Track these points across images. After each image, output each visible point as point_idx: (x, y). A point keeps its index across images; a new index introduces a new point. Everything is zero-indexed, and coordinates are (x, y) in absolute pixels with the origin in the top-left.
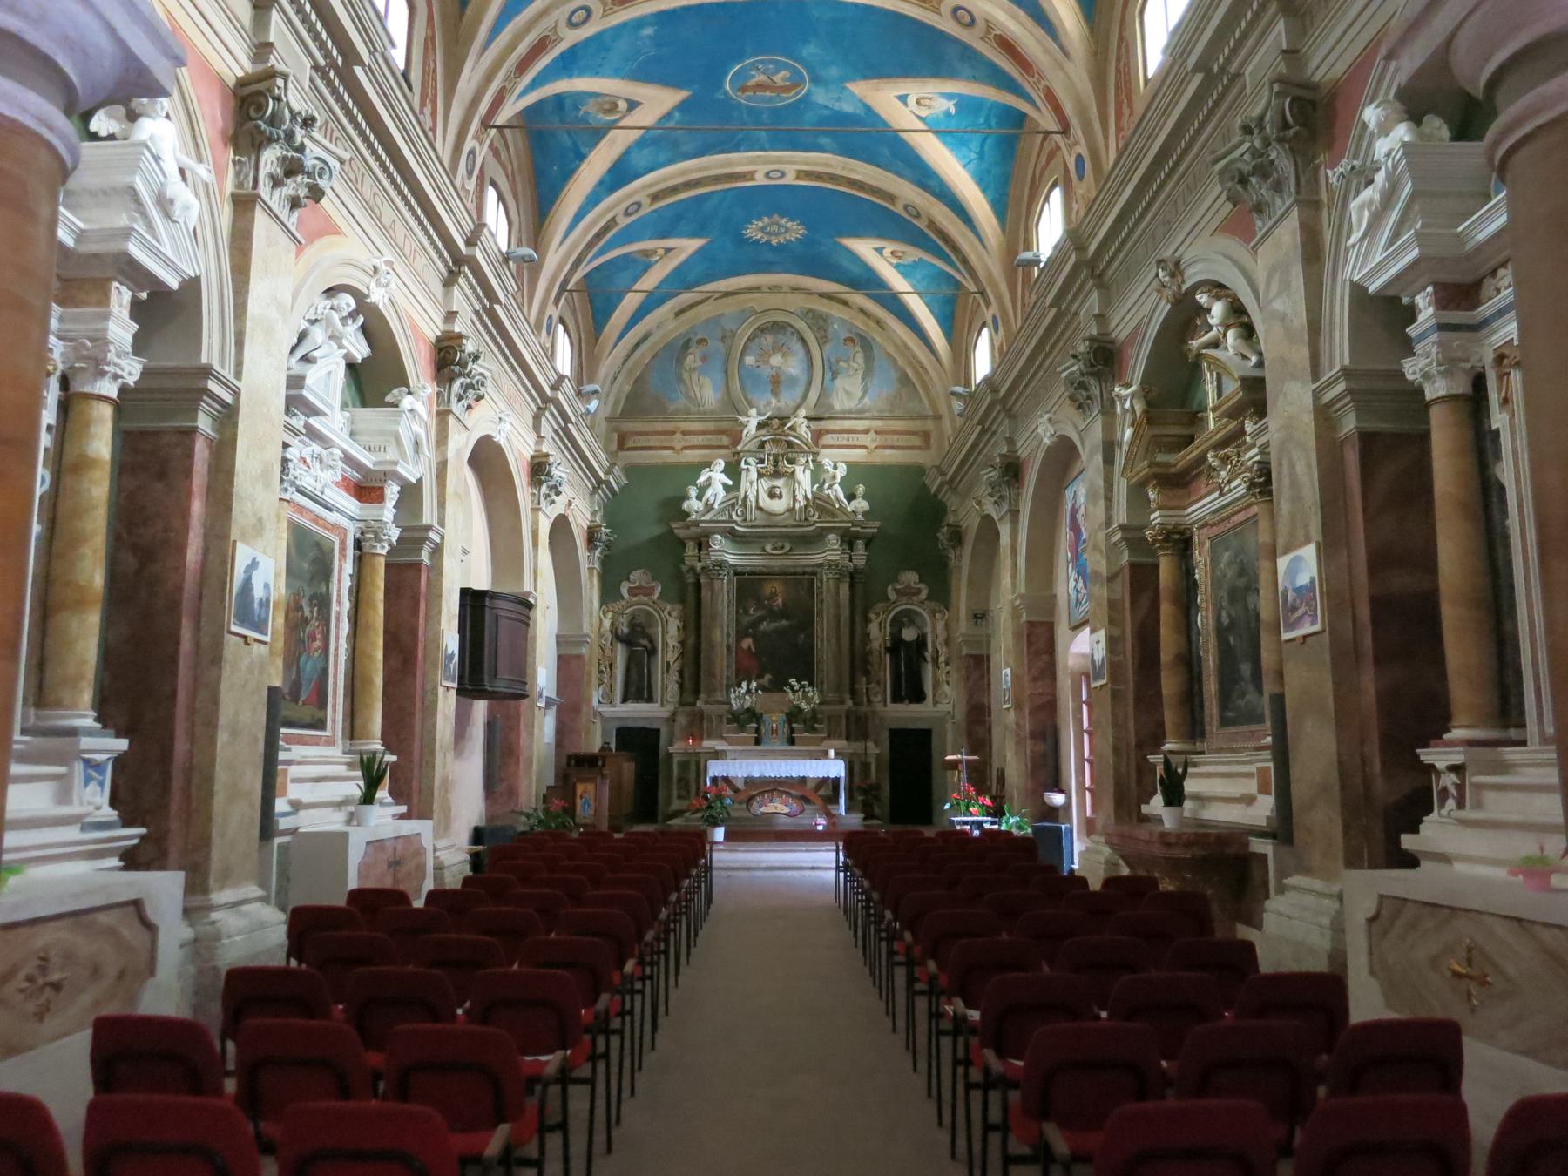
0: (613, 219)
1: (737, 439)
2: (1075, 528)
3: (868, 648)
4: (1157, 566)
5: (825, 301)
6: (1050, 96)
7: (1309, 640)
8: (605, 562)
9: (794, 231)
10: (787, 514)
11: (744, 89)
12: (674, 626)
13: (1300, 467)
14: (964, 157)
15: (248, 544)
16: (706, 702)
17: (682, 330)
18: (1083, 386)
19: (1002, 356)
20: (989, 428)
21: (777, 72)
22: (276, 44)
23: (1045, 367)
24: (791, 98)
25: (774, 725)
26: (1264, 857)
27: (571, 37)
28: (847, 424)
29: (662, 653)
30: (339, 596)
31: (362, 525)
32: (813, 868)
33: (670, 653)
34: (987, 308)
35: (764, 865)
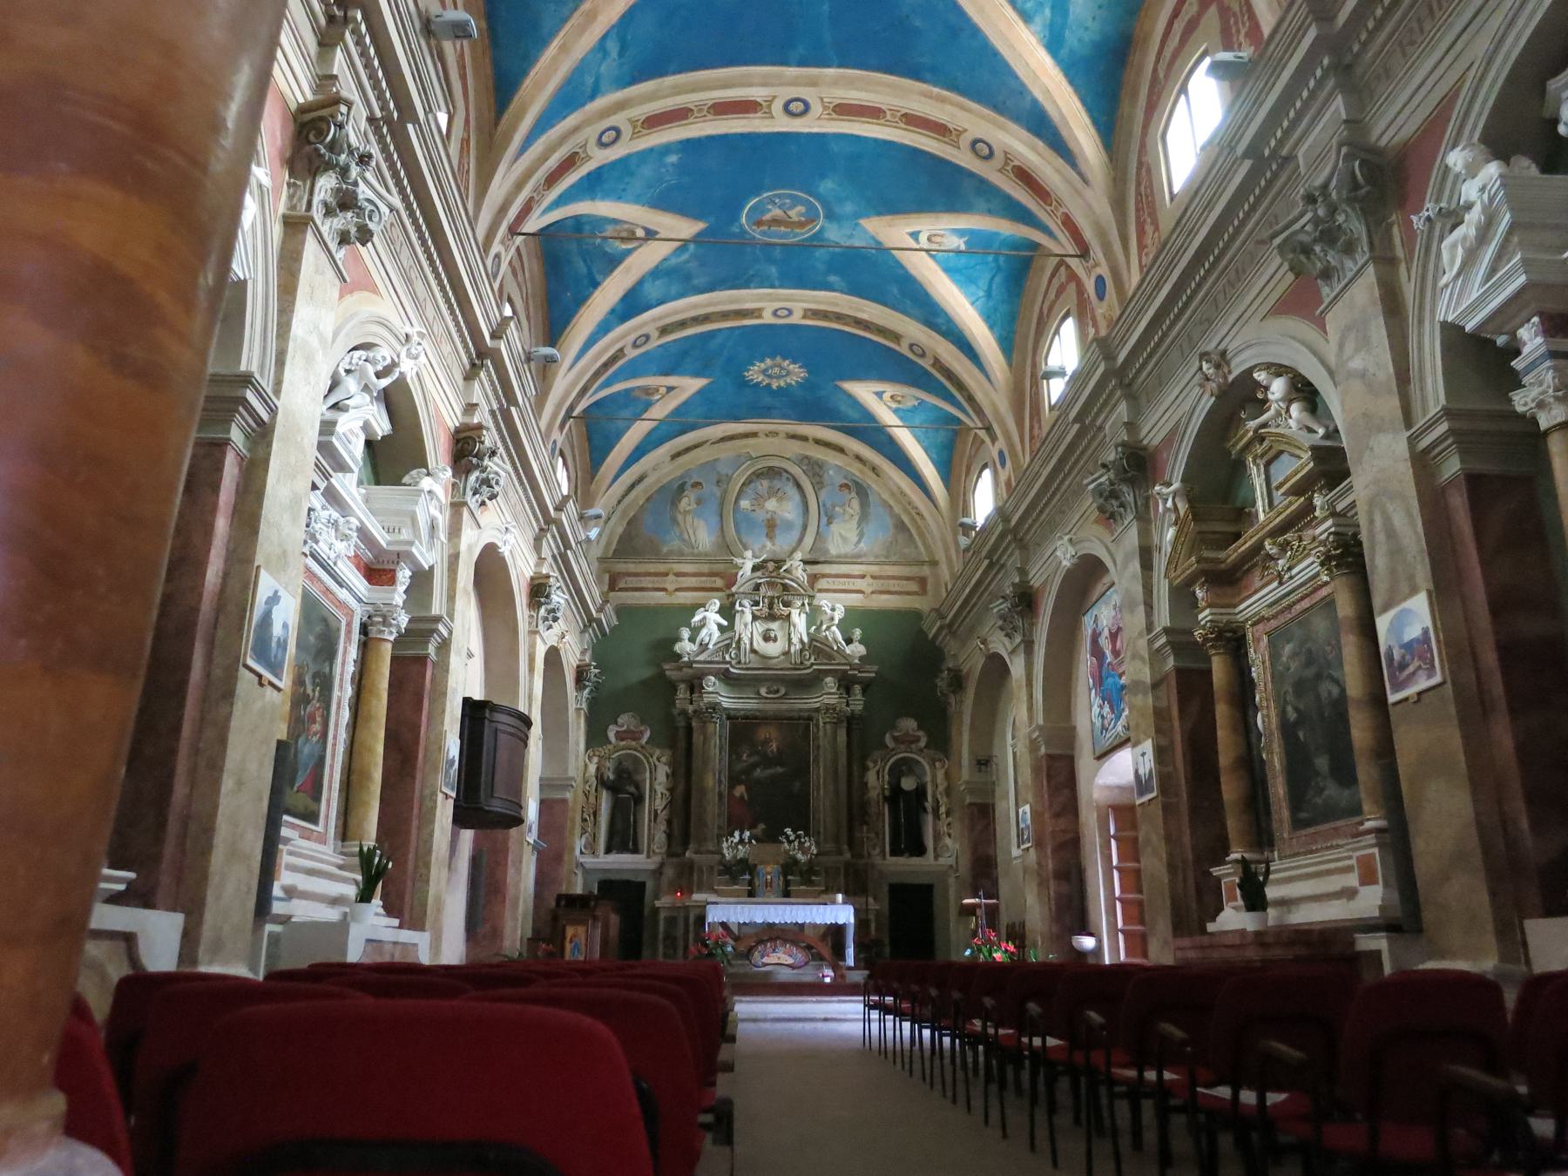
0: (621, 350)
1: (731, 581)
3: (866, 797)
5: (822, 449)
6: (1069, 224)
7: (1424, 696)
8: (593, 703)
9: (795, 373)
10: (782, 657)
11: (759, 223)
12: (663, 771)
13: (1399, 520)
14: (972, 294)
15: (271, 574)
16: (696, 853)
17: (678, 473)
18: (1114, 495)
19: (1009, 492)
20: (998, 560)
21: (792, 207)
22: (340, 78)
23: (1062, 490)
24: (804, 234)
25: (769, 877)
26: (1378, 953)
27: (600, 157)
28: (844, 569)
29: (650, 802)
30: (341, 680)
31: (369, 608)
32: (826, 1020)
33: (658, 801)
34: (993, 443)
35: (772, 1016)
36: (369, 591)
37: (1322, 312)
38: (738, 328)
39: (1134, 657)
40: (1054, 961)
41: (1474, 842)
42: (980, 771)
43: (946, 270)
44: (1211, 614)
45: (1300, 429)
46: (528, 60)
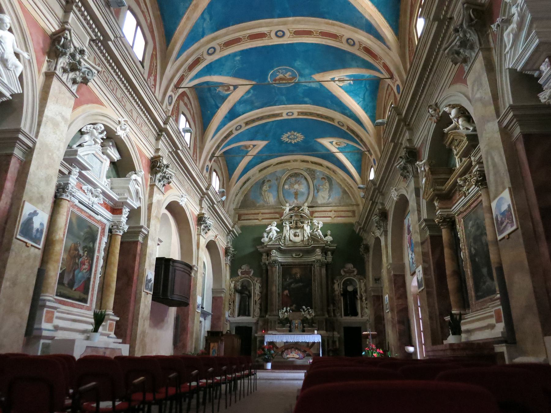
0: (231, 131)
1: (282, 215)
2: (409, 232)
4: (441, 237)
5: (314, 165)
6: (385, 66)
7: (511, 236)
9: (299, 137)
12: (258, 286)
13: (497, 159)
14: (358, 100)
16: (270, 316)
21: (286, 73)
27: (209, 59)
31: (112, 223)
33: (256, 297)
36: (113, 216)
37: (465, 77)
38: (275, 121)
39: (415, 233)
40: (399, 358)
41: (533, 301)
42: (376, 283)
43: (346, 92)
44: (440, 212)
45: (464, 129)
46: (176, 24)
